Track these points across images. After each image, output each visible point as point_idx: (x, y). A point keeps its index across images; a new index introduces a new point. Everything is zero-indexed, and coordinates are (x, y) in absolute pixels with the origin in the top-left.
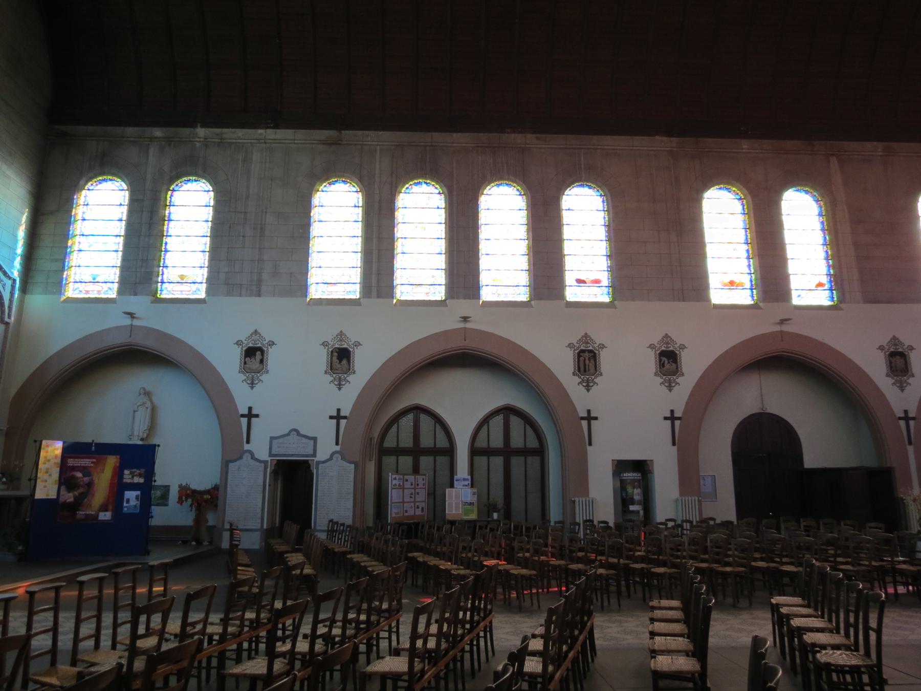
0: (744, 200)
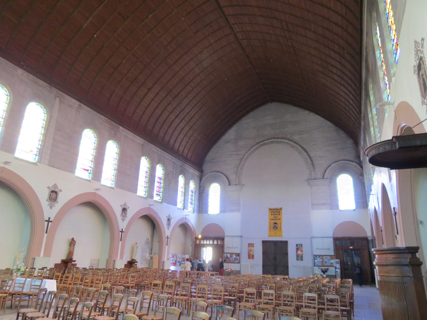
0: (9, 97)
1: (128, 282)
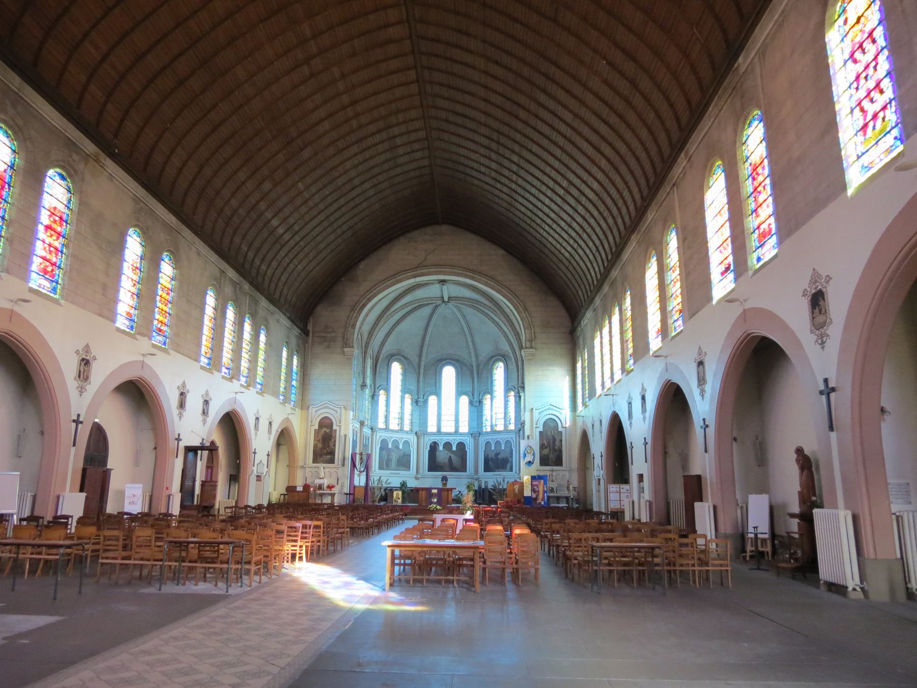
1: (97, 553)
